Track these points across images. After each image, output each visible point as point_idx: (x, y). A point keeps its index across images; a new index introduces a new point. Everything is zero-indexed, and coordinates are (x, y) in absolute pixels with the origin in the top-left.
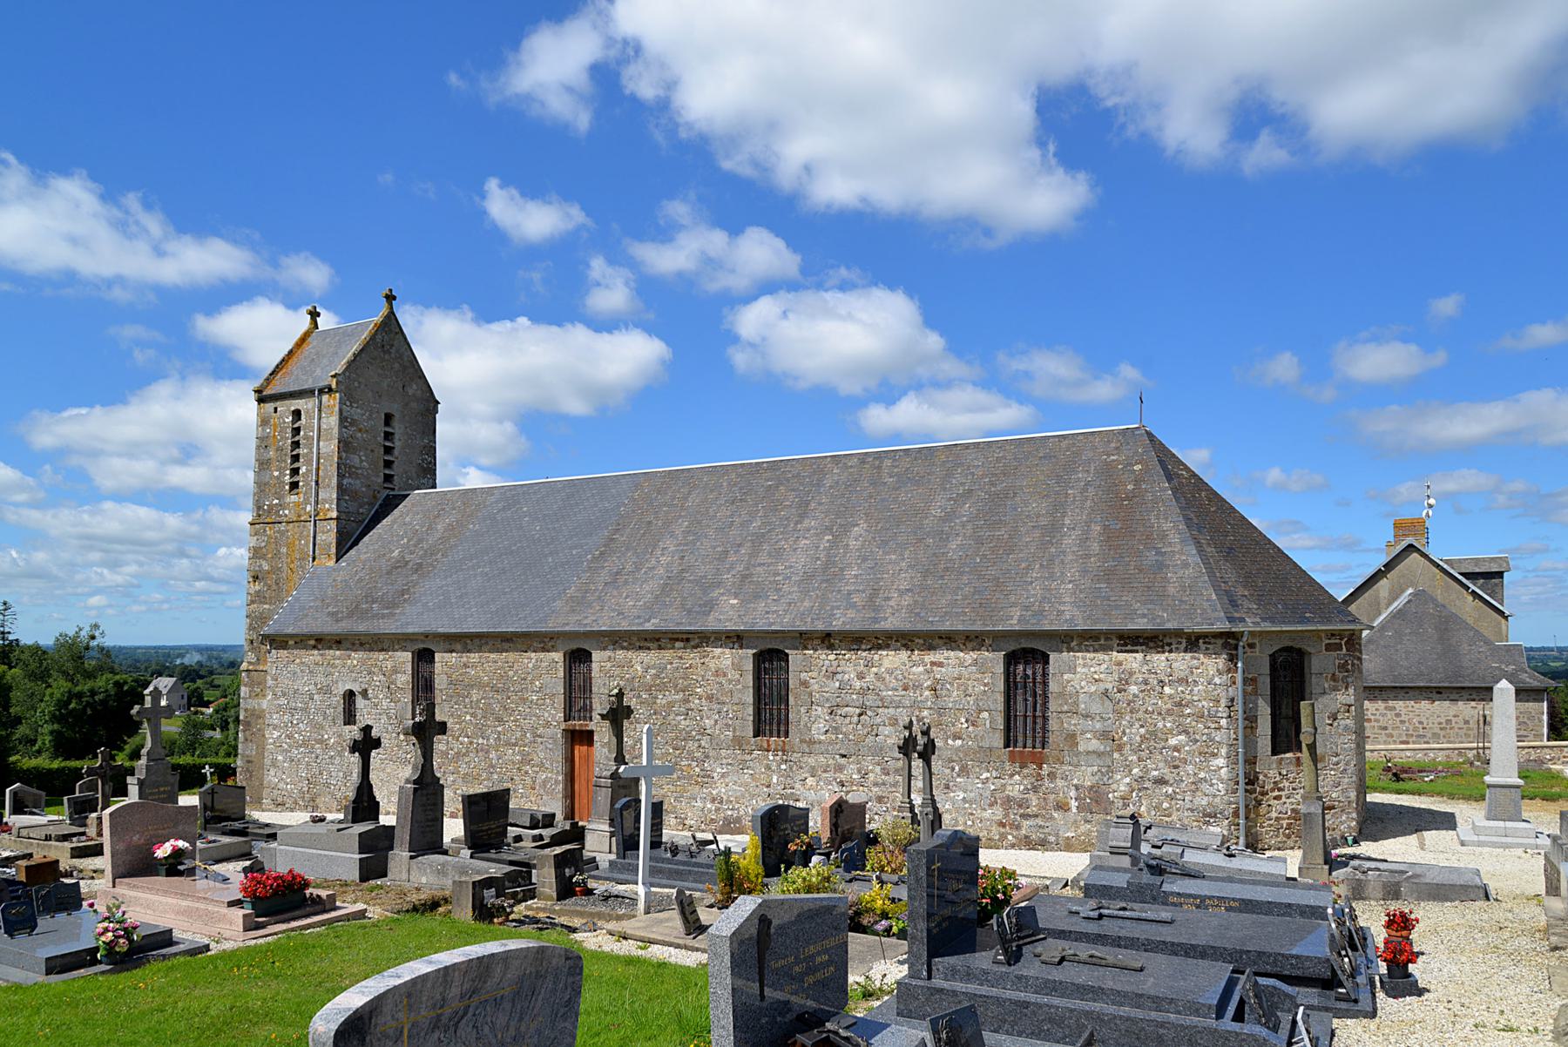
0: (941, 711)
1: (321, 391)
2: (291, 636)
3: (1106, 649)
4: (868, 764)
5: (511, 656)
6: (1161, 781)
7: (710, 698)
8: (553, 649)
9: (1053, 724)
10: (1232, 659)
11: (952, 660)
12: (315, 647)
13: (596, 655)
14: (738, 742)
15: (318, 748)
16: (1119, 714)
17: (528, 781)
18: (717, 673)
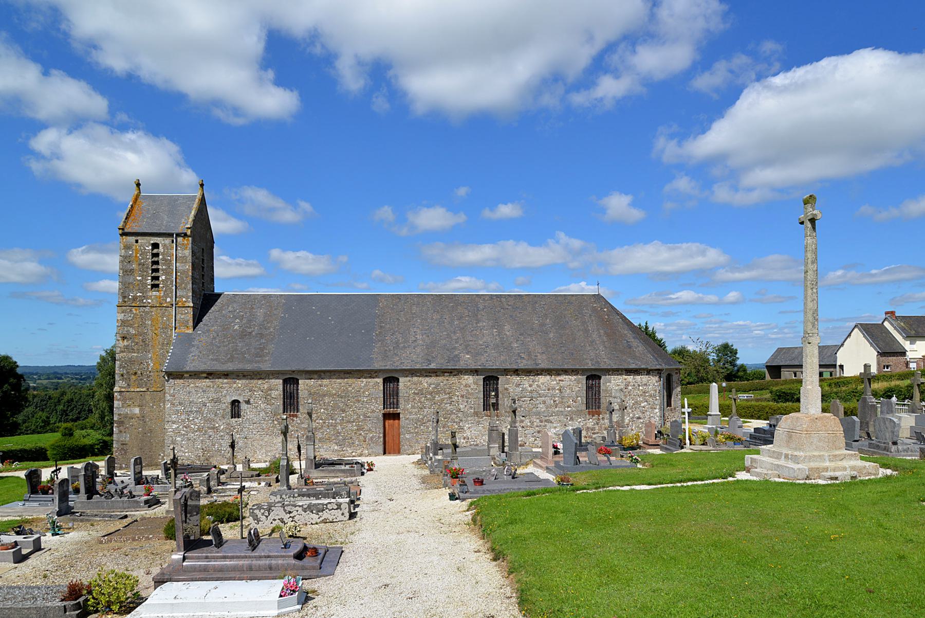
0: (563, 398)
1: (178, 235)
2: (187, 372)
3: (621, 374)
4: (534, 419)
5: (350, 381)
6: (639, 418)
7: (462, 396)
8: (377, 377)
9: (602, 400)
10: (660, 377)
11: (567, 379)
12: (206, 378)
13: (401, 379)
14: (476, 414)
15: (211, 432)
16: (626, 396)
17: (362, 438)
18: (466, 386)
